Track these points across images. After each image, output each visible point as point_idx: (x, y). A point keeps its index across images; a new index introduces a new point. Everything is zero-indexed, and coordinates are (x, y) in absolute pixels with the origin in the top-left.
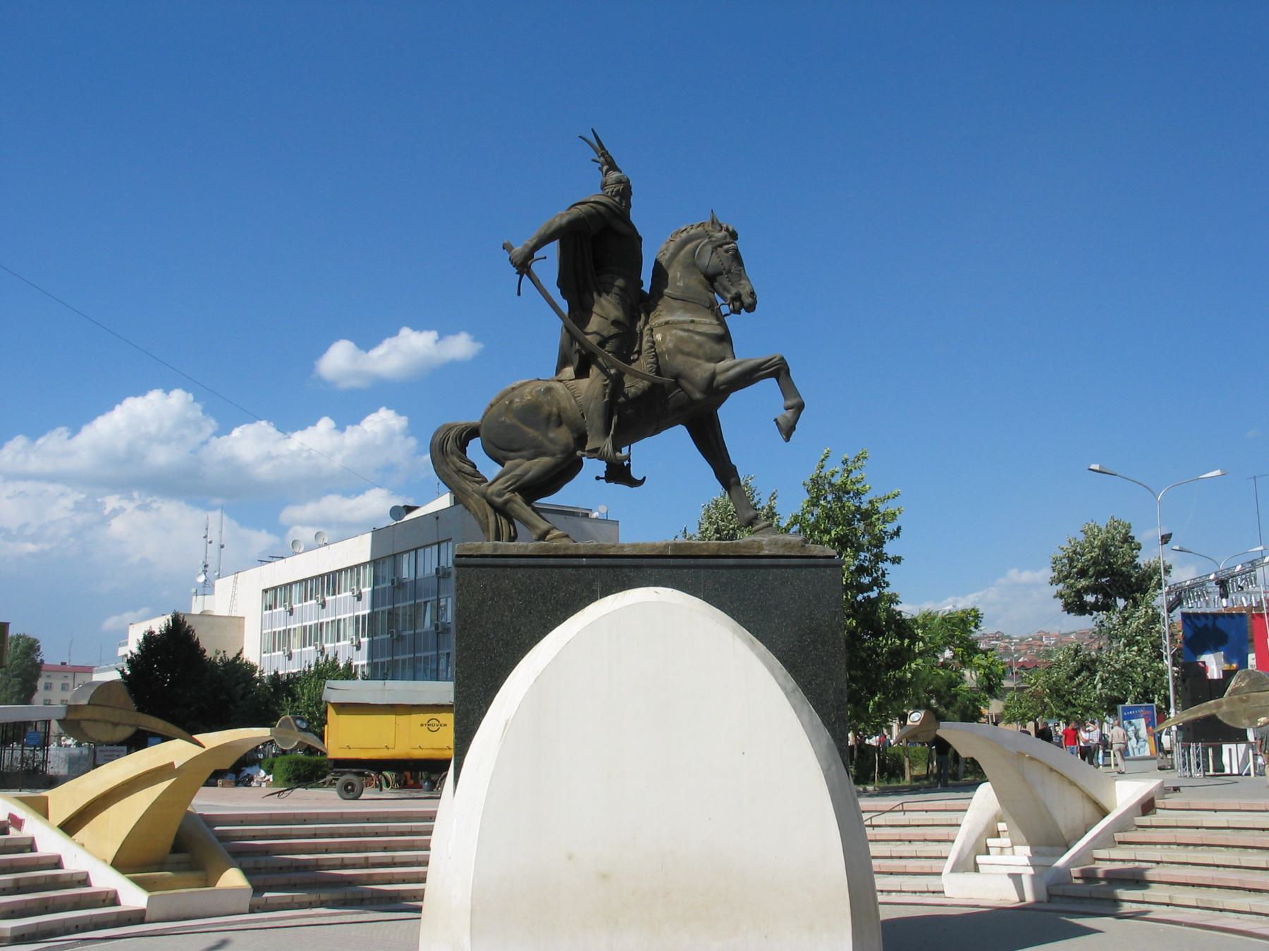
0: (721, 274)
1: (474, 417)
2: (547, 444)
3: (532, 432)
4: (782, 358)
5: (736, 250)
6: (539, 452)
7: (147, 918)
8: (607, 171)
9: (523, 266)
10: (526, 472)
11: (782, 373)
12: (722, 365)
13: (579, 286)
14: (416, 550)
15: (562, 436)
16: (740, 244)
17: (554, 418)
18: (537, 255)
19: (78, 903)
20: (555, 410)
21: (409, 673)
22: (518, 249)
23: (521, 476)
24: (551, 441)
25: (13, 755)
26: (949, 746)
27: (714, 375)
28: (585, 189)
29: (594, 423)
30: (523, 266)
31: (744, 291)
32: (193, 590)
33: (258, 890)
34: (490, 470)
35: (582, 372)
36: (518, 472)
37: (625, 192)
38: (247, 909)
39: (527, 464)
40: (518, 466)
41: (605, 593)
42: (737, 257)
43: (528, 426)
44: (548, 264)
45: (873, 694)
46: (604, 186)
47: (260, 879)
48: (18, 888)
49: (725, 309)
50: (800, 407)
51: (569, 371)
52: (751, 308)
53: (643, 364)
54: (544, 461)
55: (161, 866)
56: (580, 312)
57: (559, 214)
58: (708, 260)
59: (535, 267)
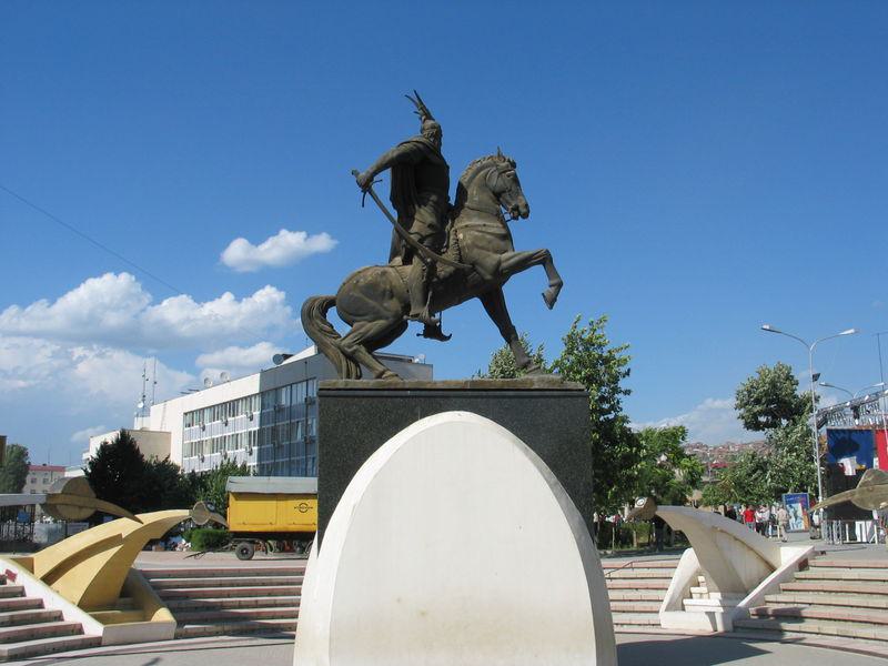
0: (504, 192)
3: (372, 303)
7: (103, 643)
9: (366, 186)
13: (405, 200)
15: (393, 305)
16: (519, 171)
19: (55, 633)
29: (416, 295)
30: (366, 186)
34: (343, 329)
38: (173, 637)
39: (369, 325)
40: (362, 326)
42: (516, 180)
44: (384, 185)
46: (422, 130)
48: (12, 622)
49: (507, 217)
50: (560, 285)
51: (398, 260)
55: (112, 606)
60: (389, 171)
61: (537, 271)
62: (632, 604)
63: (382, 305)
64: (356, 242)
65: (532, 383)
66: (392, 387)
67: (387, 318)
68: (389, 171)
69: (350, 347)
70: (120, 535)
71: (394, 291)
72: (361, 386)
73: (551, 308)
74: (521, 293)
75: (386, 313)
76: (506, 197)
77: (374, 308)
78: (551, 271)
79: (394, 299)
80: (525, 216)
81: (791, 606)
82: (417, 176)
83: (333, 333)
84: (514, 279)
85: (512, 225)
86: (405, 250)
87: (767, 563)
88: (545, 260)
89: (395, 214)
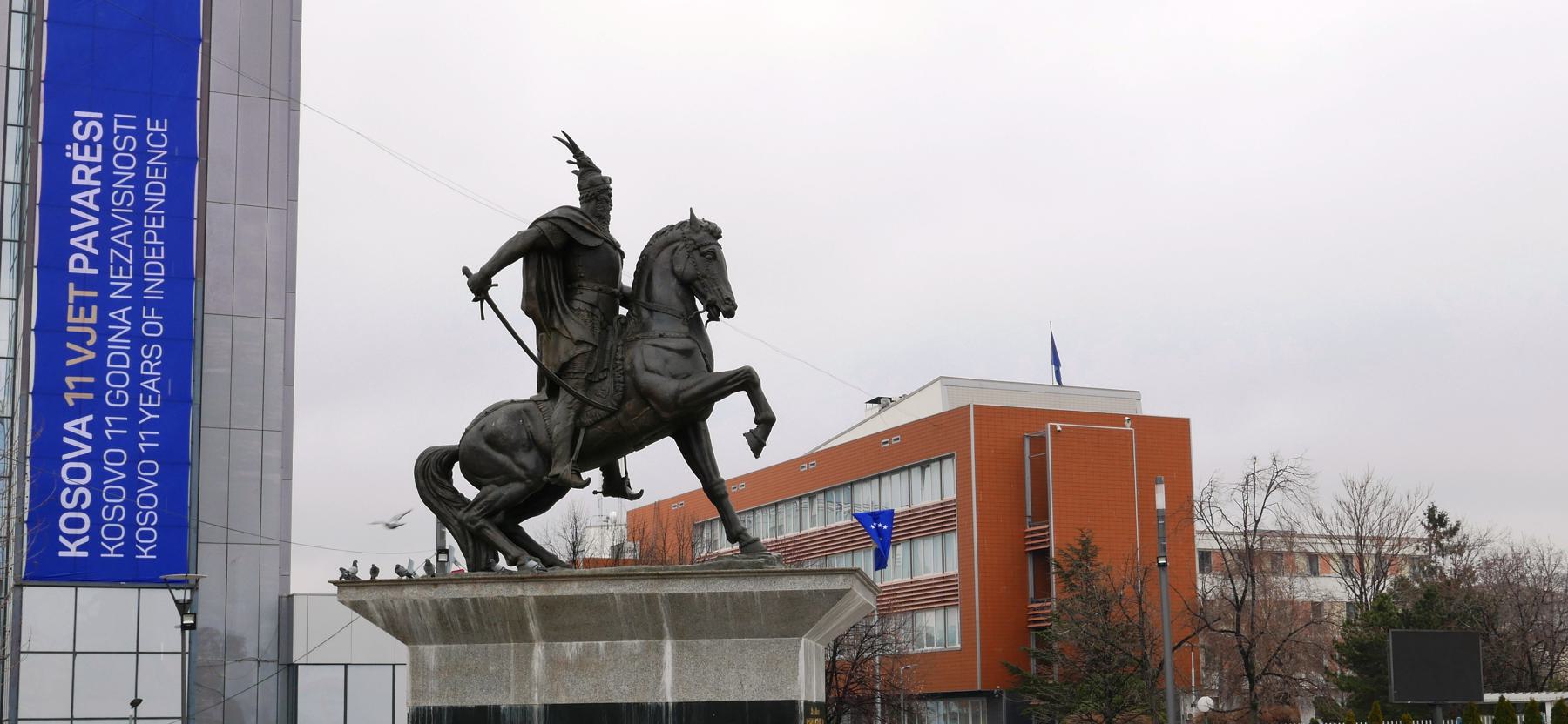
1: (453, 438)
2: (517, 469)
6: (511, 478)
9: (480, 286)
10: (496, 499)
12: (690, 381)
21: (713, 267)
22: (475, 270)
24: (522, 466)
25: (249, 686)
26: (387, 629)
27: (678, 392)
30: (480, 286)
34: (469, 491)
44: (510, 284)
45: (1061, 607)
52: (730, 314)
54: (515, 488)
57: (518, 221)
58: (684, 266)
61: (740, 399)
74: (728, 421)
75: (522, 473)
80: (730, 314)
88: (746, 381)
89: (527, 329)
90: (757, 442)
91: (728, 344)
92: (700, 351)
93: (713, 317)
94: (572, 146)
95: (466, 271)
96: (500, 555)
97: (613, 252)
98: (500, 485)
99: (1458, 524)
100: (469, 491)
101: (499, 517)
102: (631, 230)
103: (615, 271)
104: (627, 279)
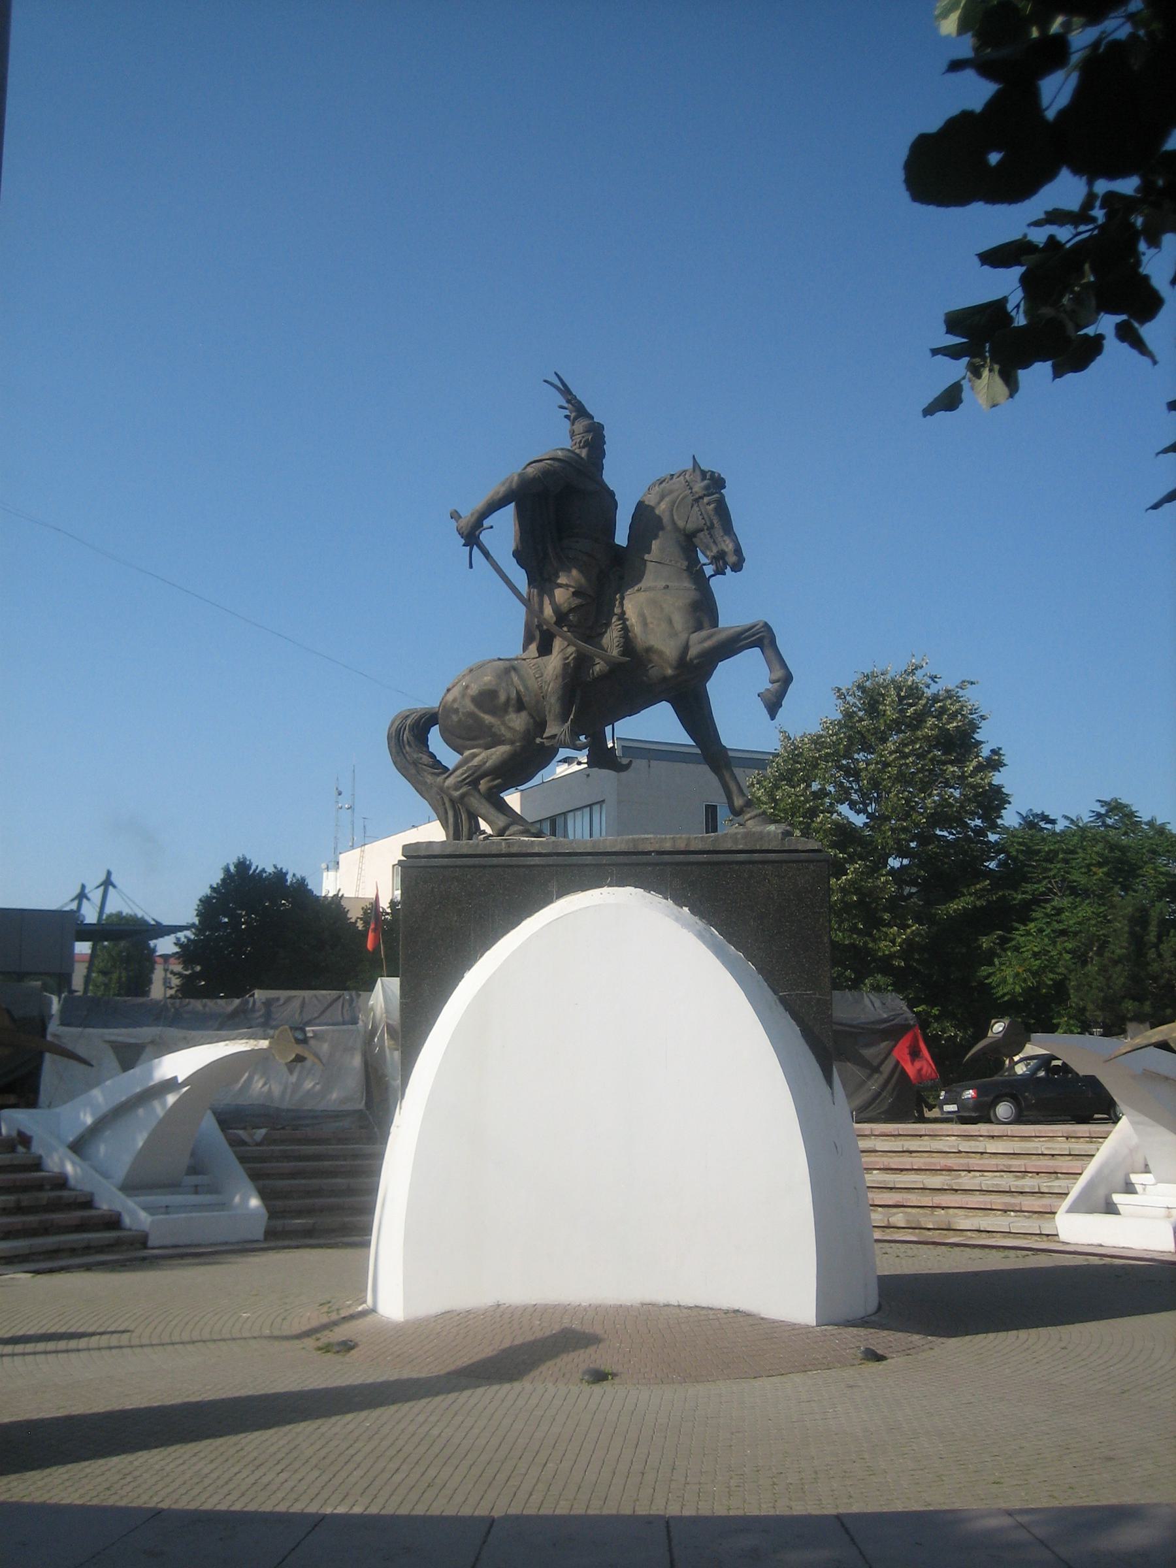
0: (702, 530)
3: (488, 718)
4: (766, 625)
5: (723, 497)
7: (150, 1244)
8: (576, 418)
9: (471, 537)
11: (766, 642)
13: (539, 555)
14: (590, 806)
15: (518, 722)
16: (730, 495)
17: (513, 702)
18: (486, 523)
19: (81, 1227)
20: (514, 695)
23: (478, 767)
28: (554, 438)
29: (553, 704)
30: (471, 537)
31: (729, 547)
32: (324, 866)
33: (273, 1214)
34: (449, 757)
35: (545, 650)
36: (475, 762)
37: (595, 439)
38: (261, 1236)
39: (484, 754)
40: (474, 756)
41: (559, 896)
42: (722, 510)
43: (485, 712)
44: (503, 531)
46: (572, 434)
47: (279, 1204)
48: (19, 1210)
49: (709, 570)
50: (788, 679)
51: (533, 647)
53: (611, 639)
55: (172, 1186)
56: (541, 579)
59: (485, 537)
60: (510, 510)
61: (752, 657)
62: (930, 1233)
63: (504, 723)
64: (477, 624)
65: (736, 841)
66: (423, 853)
67: (512, 743)
68: (510, 510)
69: (456, 789)
70: (175, 1078)
71: (525, 699)
72: (465, 851)
73: (773, 717)
74: (734, 691)
75: (508, 735)
76: (702, 530)
77: (491, 726)
78: (775, 657)
79: (524, 714)
80: (737, 567)
81: (1107, 1261)
82: (562, 520)
83: (437, 766)
84: (723, 667)
85: (716, 584)
86: (541, 637)
87: (1147, 1165)
88: (761, 638)
89: (520, 577)
90: (773, 705)
91: (737, 602)
92: (704, 609)
93: (720, 572)
94: (566, 391)
95: (455, 515)
96: (480, 820)
97: (608, 500)
98: (487, 748)
99: (1119, 1214)
100: (449, 757)
101: (483, 785)
102: (629, 480)
103: (610, 528)
104: (621, 538)
